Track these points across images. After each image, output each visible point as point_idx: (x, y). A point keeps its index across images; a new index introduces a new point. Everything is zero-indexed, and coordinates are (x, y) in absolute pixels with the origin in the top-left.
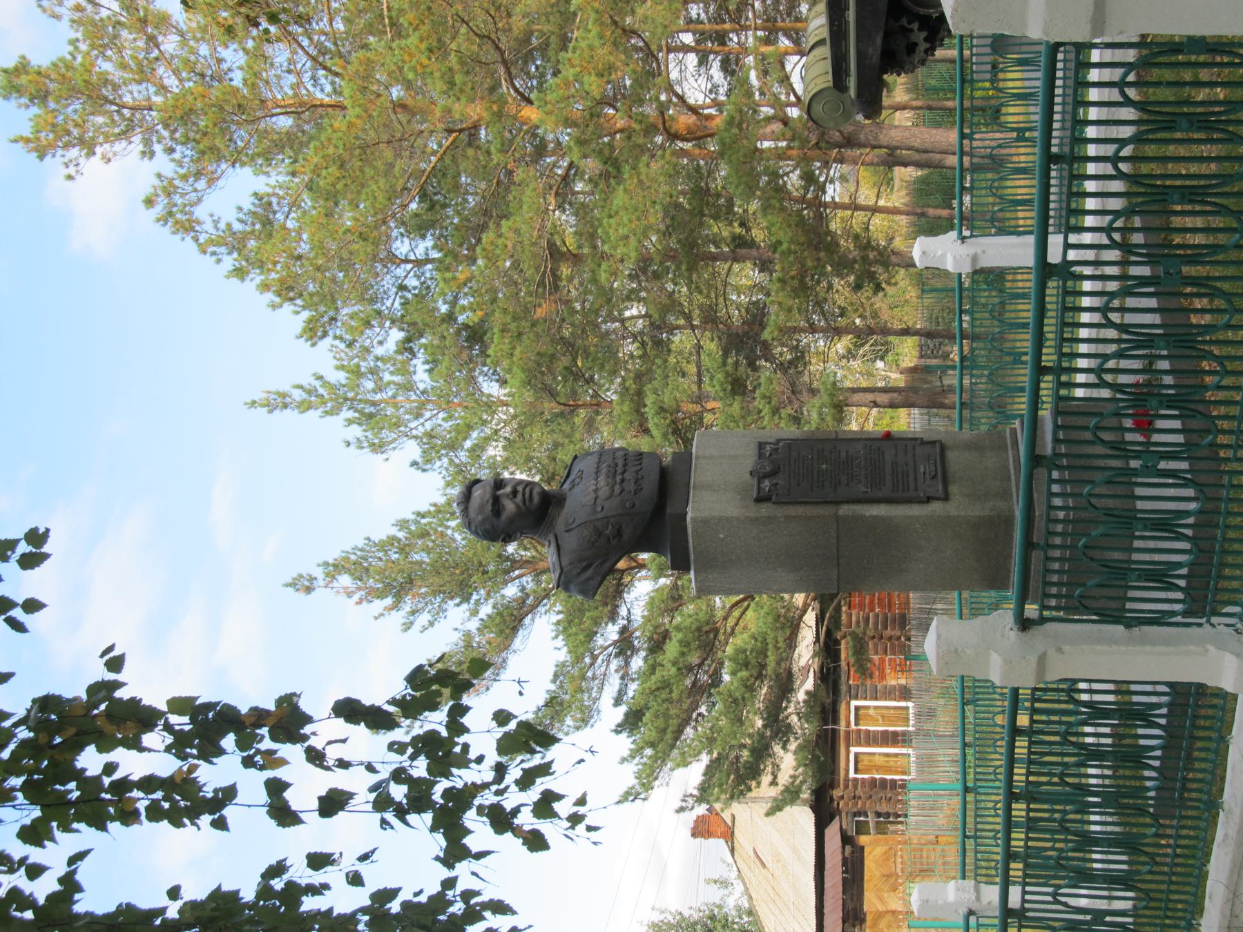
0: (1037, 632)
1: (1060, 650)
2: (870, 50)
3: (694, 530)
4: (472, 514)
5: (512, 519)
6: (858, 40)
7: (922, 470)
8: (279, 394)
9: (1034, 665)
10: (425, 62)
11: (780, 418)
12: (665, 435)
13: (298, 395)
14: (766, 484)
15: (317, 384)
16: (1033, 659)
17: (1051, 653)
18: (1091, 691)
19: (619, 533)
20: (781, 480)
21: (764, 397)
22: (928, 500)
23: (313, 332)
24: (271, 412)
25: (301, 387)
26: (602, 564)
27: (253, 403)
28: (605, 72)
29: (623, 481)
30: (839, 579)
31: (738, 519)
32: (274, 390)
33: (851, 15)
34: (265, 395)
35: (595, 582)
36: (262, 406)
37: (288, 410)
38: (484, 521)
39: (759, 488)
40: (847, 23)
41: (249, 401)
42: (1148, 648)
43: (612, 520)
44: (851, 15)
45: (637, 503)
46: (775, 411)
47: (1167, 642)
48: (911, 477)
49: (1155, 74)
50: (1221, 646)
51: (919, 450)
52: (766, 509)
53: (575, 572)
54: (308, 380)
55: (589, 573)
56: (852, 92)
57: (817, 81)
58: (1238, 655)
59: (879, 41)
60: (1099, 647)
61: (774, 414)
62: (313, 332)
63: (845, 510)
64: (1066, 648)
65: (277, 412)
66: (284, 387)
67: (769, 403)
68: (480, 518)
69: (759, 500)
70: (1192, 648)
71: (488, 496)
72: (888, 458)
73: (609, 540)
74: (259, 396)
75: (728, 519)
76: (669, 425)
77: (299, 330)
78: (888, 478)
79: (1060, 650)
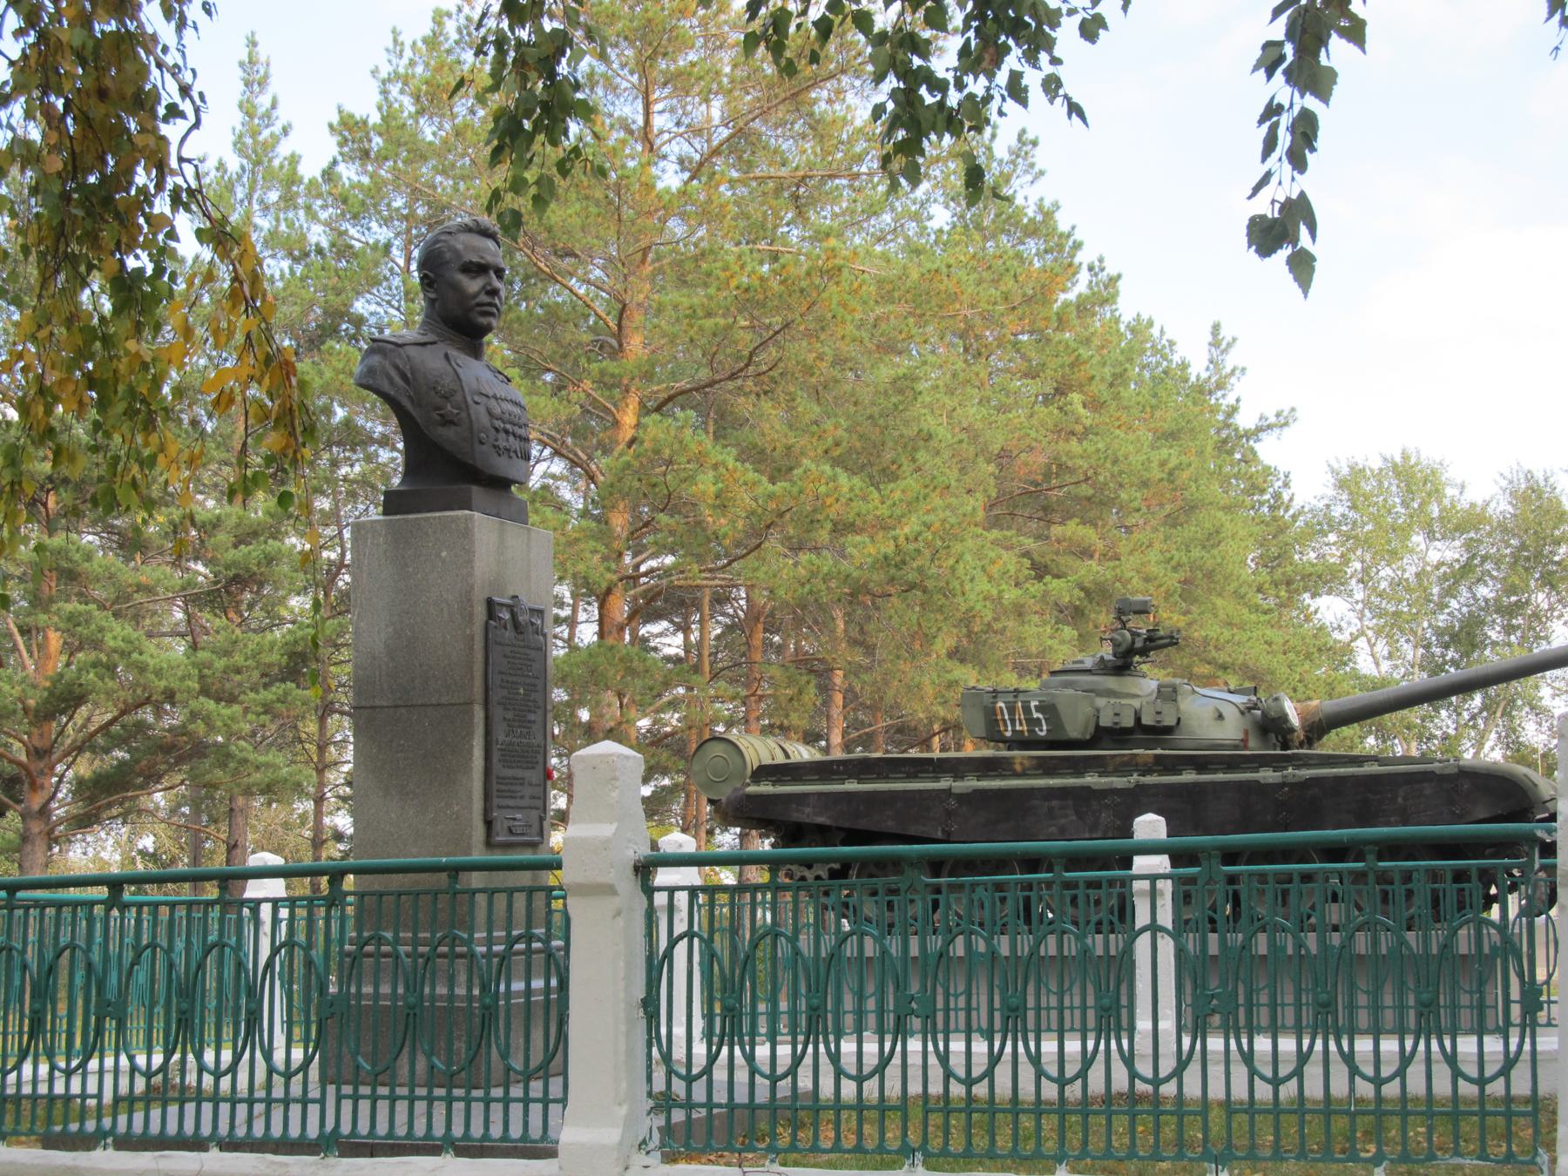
0: (628, 885)
1: (618, 913)
2: (808, 810)
3: (454, 519)
4: (464, 237)
5: (456, 288)
6: (820, 794)
7: (519, 816)
8: (266, 76)
9: (601, 879)
10: (733, 283)
11: (258, 715)
12: (234, 563)
13: (264, 102)
14: (506, 616)
15: (277, 129)
16: (610, 877)
17: (616, 902)
18: (101, 1072)
19: (447, 422)
20: (509, 634)
21: (286, 694)
22: (489, 823)
23: (349, 130)
24: (241, 64)
25: (274, 106)
26: (409, 397)
27: (253, 44)
28: (722, 503)
29: (507, 432)
30: (373, 707)
31: (471, 575)
32: (272, 70)
33: (851, 786)
34: (263, 59)
35: (386, 387)
36: (250, 55)
37: (243, 87)
38: (456, 252)
39: (502, 605)
40: (842, 781)
41: (257, 38)
42: (623, 1028)
43: (464, 415)
44: (851, 786)
45: (484, 448)
46: (267, 709)
47: (630, 1052)
48: (511, 802)
49: (935, 1119)
50: (629, 1121)
51: (534, 814)
52: (480, 611)
53: (398, 361)
54: (283, 116)
55: (397, 379)
56: (752, 789)
57: (751, 750)
58: (621, 1143)
59: (820, 820)
60: (622, 964)
61: (264, 705)
62: (349, 130)
63: (479, 713)
64: (620, 922)
65: (240, 73)
66: (274, 87)
67: (279, 700)
68: (460, 247)
69: (490, 603)
70: (624, 1085)
71: (490, 259)
72: (527, 774)
73: (439, 408)
74: (263, 52)
75: (470, 562)
76: (248, 570)
77: (349, 108)
78: (510, 773)
79: (618, 913)
